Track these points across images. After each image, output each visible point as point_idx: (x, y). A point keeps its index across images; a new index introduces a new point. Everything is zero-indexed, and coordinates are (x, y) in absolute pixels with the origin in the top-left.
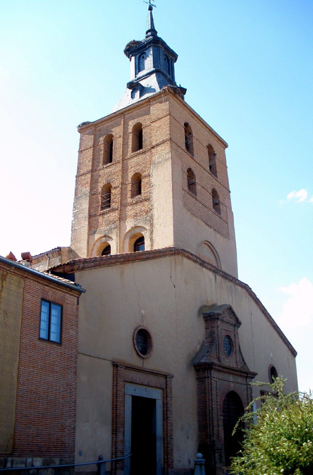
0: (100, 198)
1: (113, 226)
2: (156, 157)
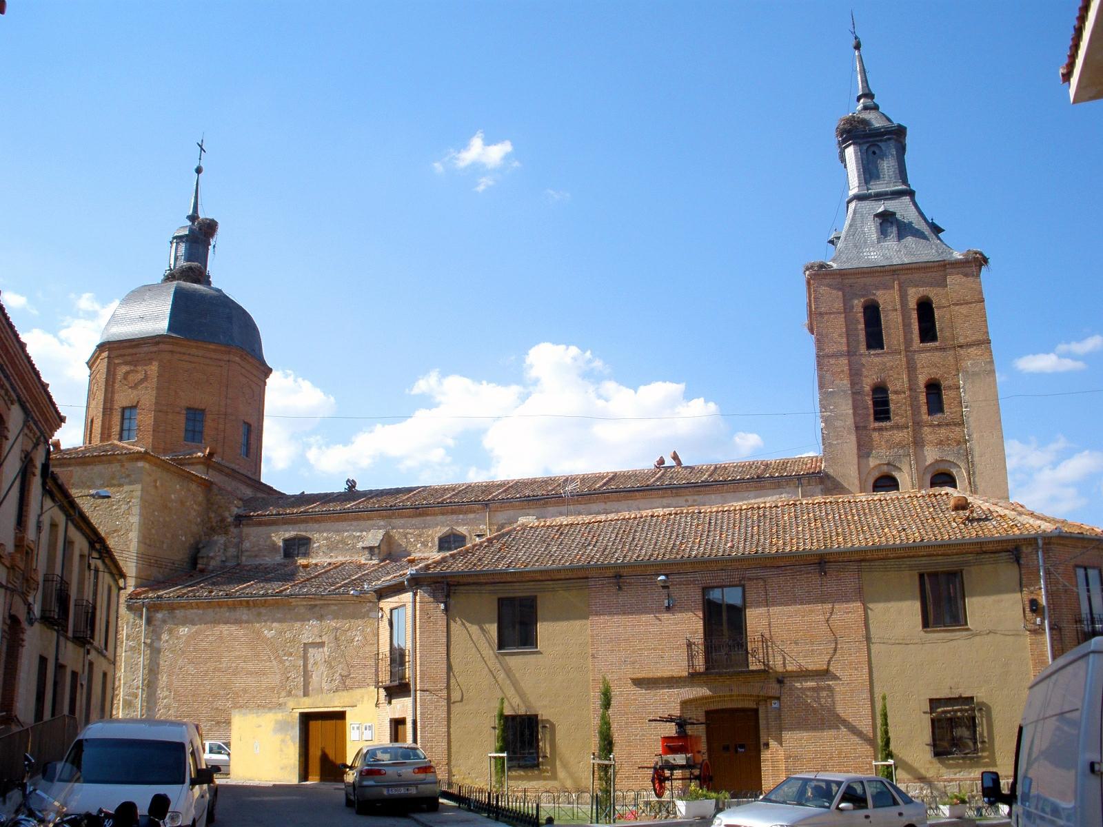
0: (870, 403)
1: (901, 452)
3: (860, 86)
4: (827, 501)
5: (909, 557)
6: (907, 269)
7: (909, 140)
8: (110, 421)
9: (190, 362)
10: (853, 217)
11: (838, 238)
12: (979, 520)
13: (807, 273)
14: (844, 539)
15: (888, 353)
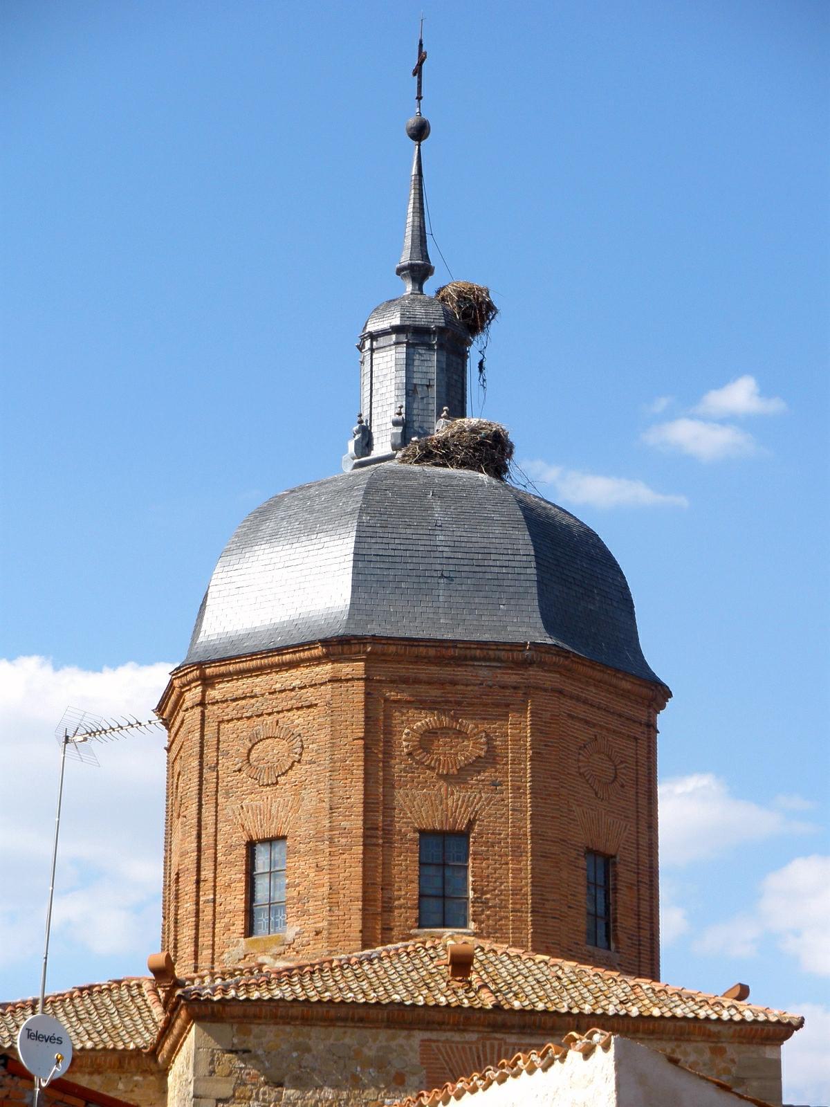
8: (387, 866)
9: (587, 722)
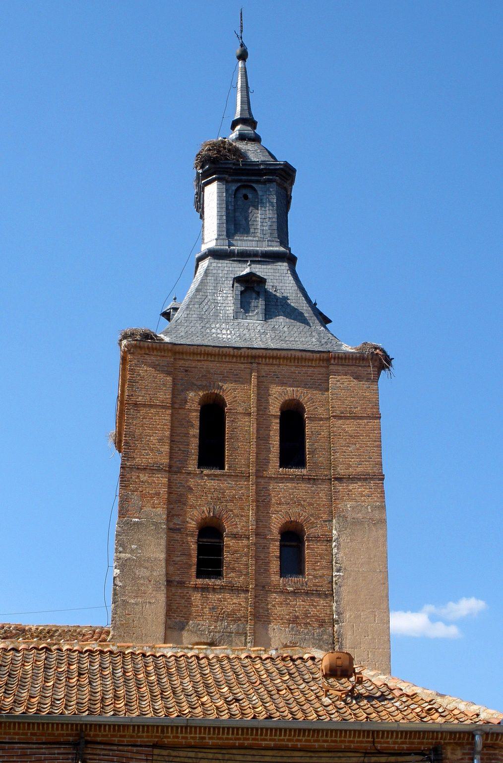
0: (194, 546)
1: (233, 627)
2: (348, 506)
3: (239, 108)
4: (106, 650)
5: (241, 747)
6: (273, 358)
7: (296, 191)
10: (202, 280)
11: (175, 309)
12: (370, 698)
13: (125, 342)
14: (126, 705)
15: (229, 476)
